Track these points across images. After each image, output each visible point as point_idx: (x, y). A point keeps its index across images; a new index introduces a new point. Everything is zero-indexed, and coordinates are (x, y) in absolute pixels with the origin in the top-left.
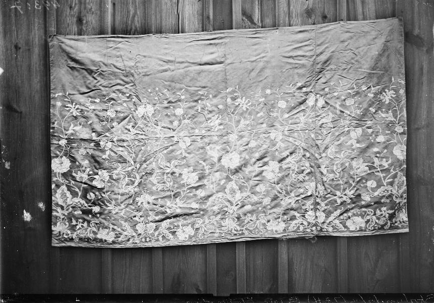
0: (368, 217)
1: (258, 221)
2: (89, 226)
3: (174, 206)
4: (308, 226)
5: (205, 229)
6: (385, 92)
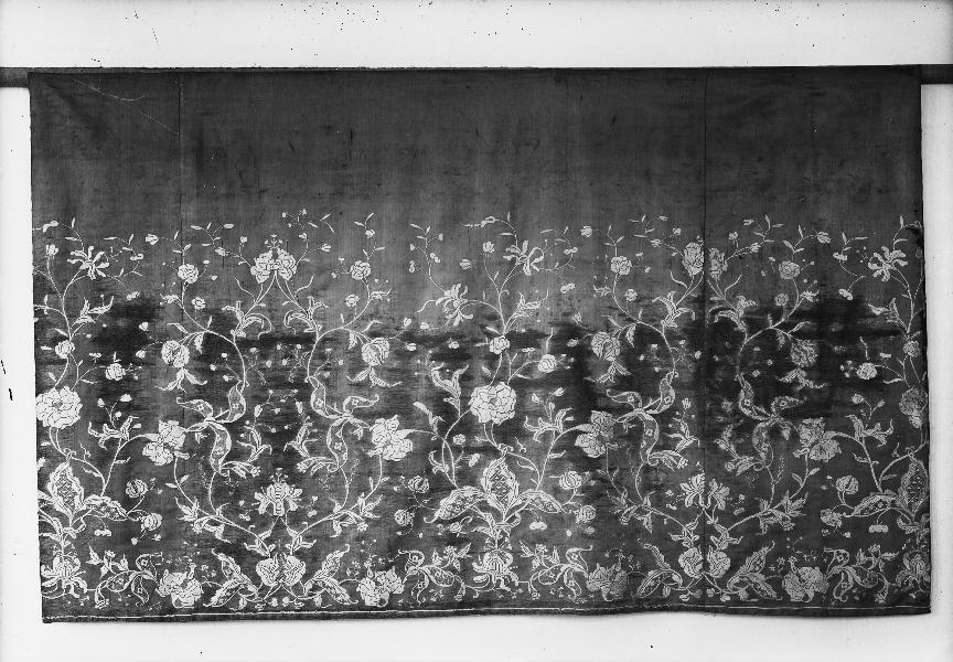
0: (836, 570)
1: (565, 567)
2: (132, 567)
3: (352, 514)
4: (684, 585)
5: (432, 578)
6: (882, 253)
